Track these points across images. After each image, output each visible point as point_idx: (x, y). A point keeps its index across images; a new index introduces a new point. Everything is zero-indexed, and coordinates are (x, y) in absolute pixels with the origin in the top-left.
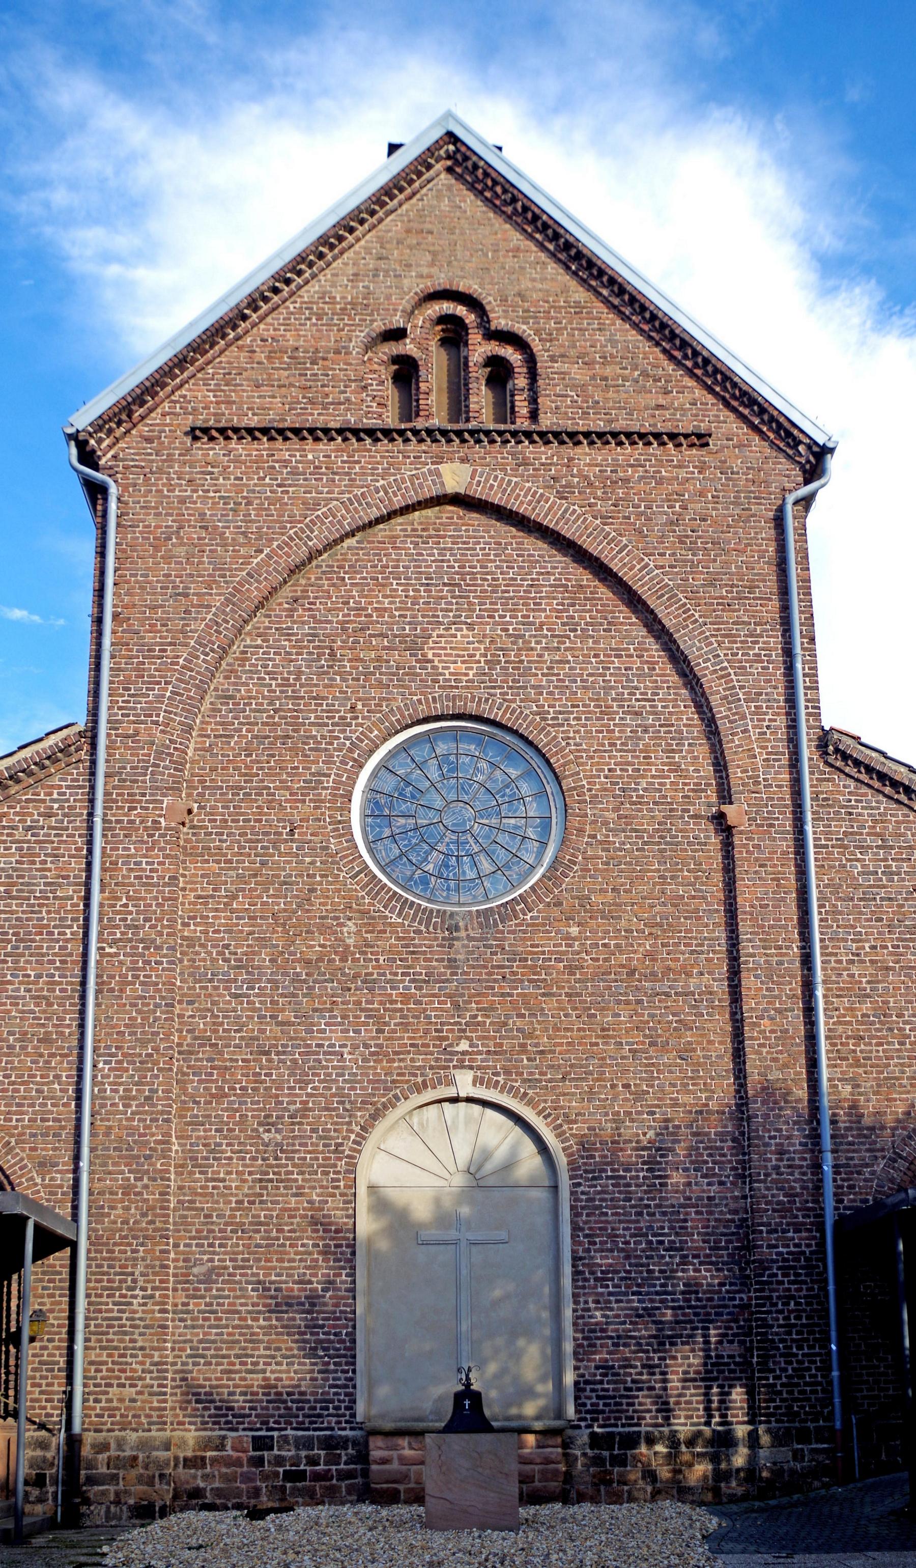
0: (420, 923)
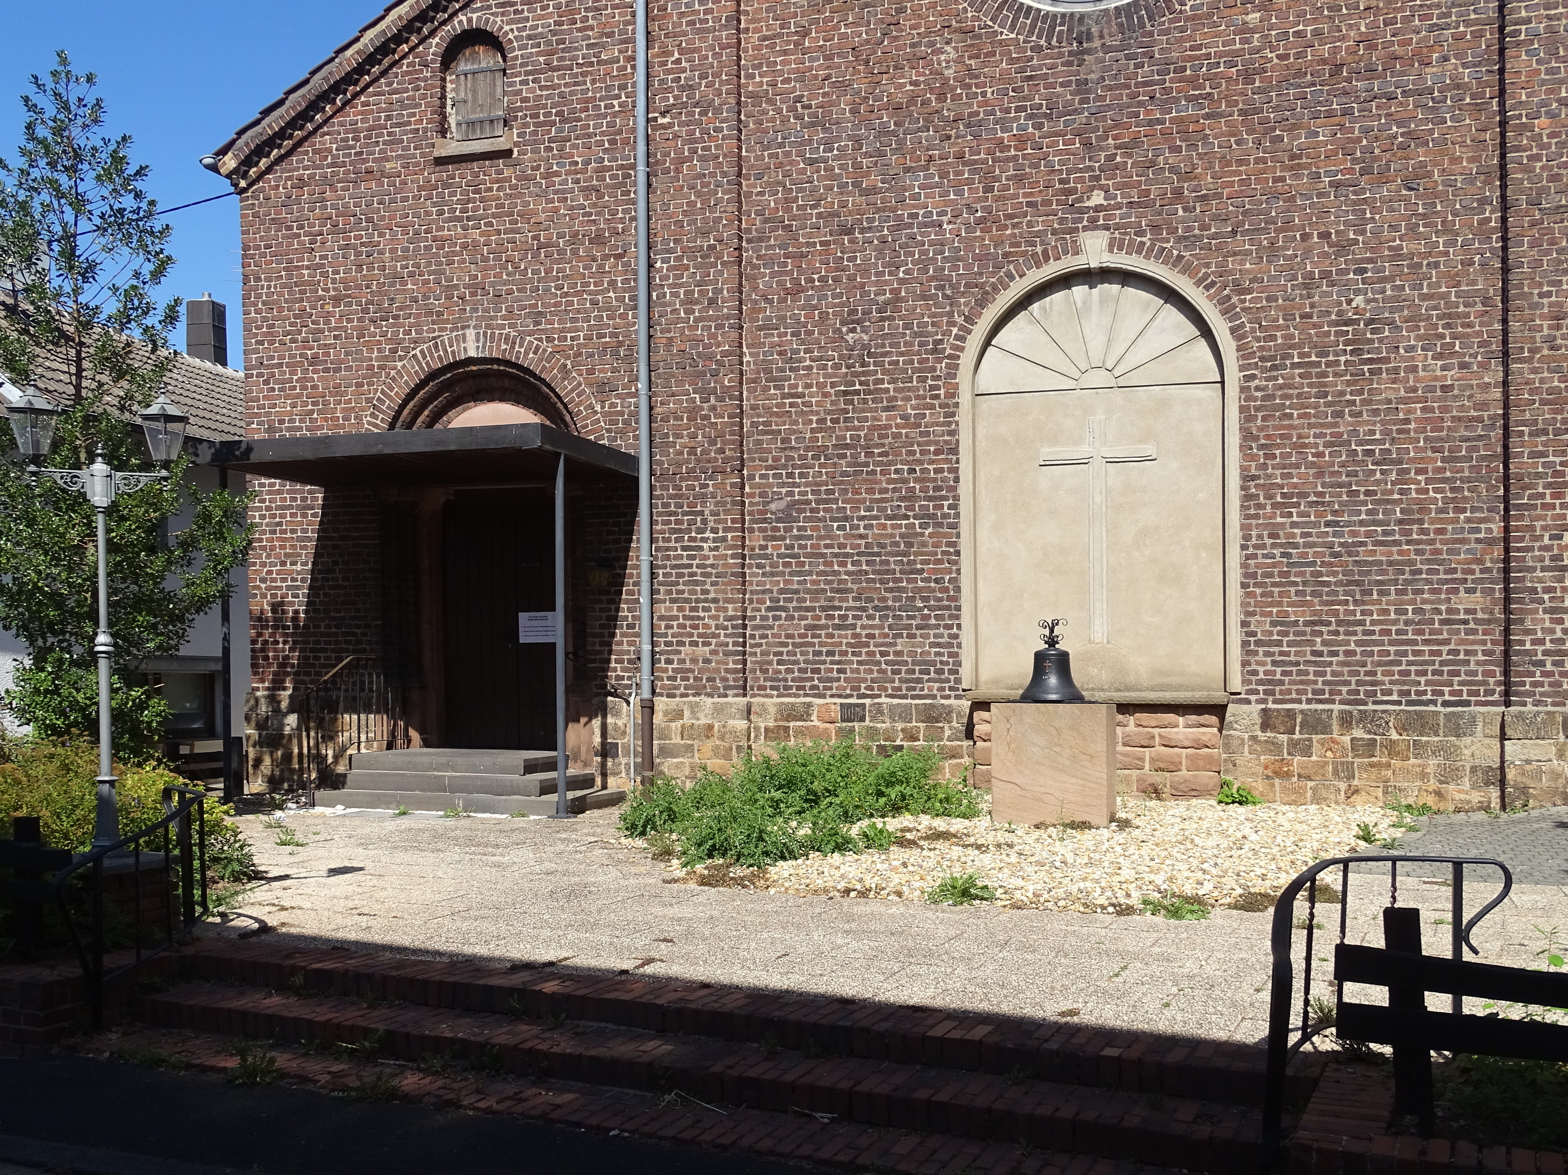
0: (1040, 37)
